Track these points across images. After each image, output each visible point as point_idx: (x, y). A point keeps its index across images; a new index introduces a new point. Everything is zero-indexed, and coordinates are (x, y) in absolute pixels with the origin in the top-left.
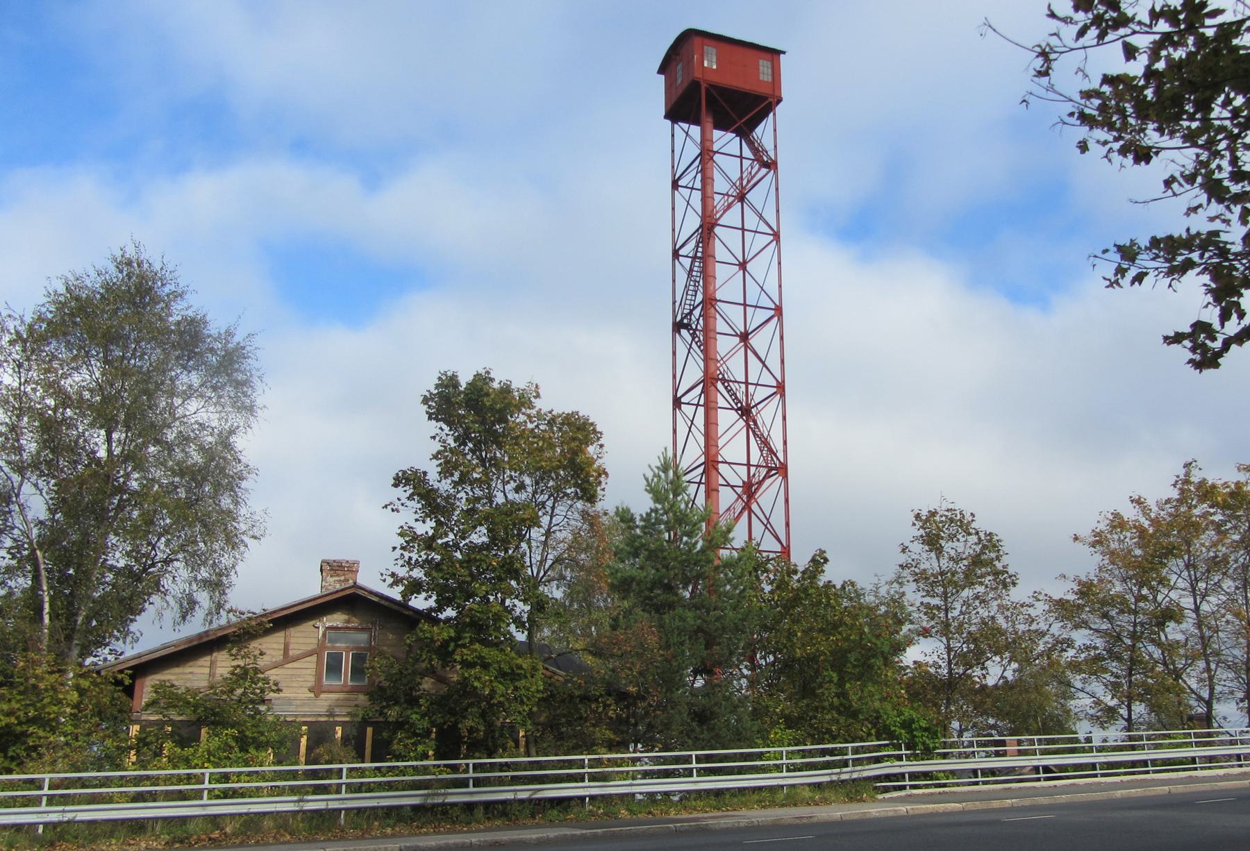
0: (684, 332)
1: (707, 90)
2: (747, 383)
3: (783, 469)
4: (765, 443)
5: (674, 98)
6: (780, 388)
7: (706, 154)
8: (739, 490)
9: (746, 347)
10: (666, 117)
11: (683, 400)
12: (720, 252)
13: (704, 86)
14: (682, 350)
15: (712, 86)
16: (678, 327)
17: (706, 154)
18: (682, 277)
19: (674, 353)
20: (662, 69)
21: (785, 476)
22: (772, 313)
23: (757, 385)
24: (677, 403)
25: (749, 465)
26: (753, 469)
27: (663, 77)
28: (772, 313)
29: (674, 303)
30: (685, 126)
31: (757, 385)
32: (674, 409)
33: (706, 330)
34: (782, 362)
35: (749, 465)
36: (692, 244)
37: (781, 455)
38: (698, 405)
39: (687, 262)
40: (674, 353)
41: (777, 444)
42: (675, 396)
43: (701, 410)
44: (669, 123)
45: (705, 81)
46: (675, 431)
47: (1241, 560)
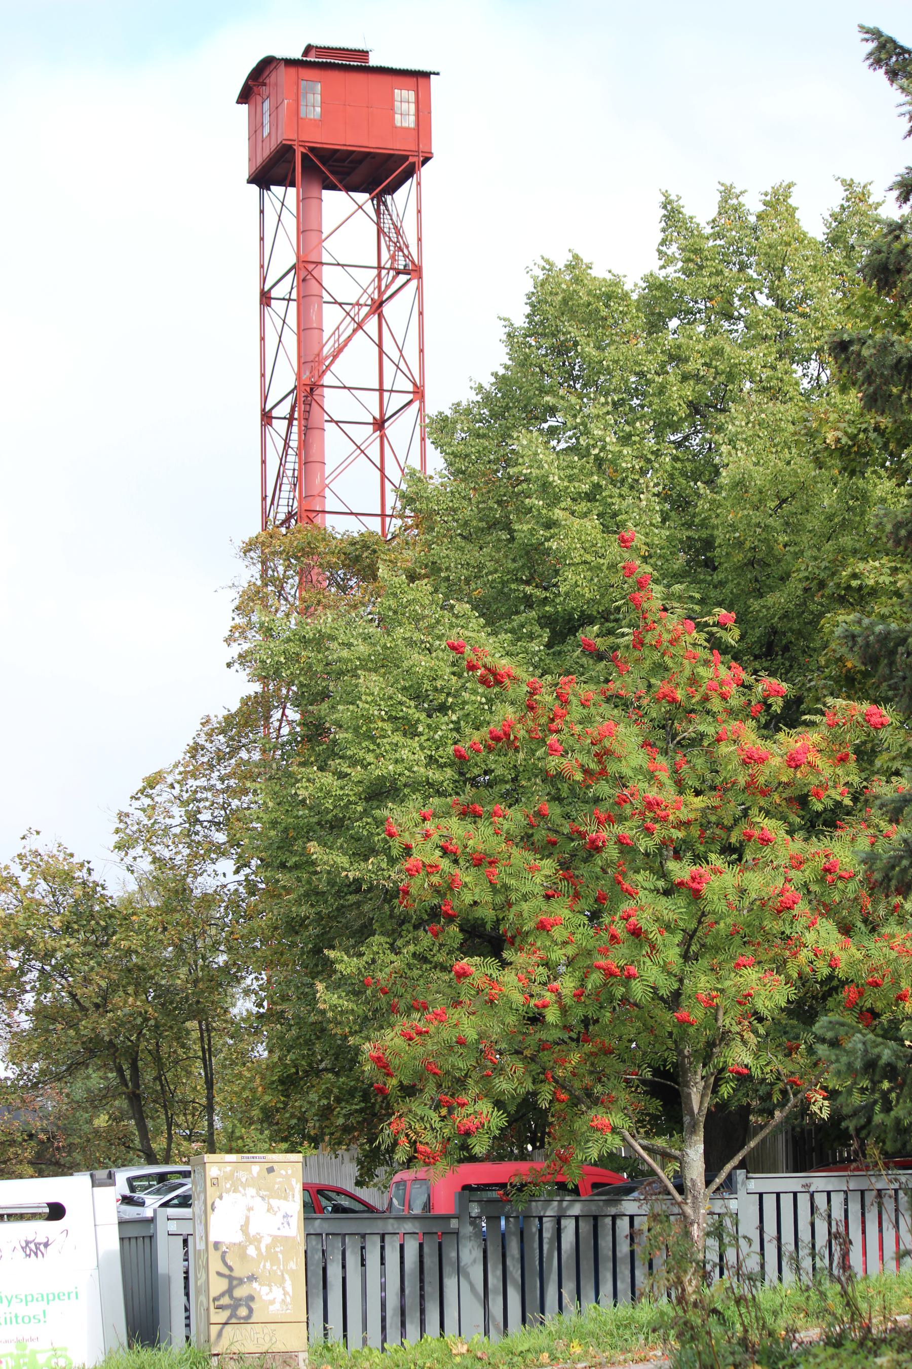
1: (304, 156)
3: (414, 271)
5: (259, 161)
7: (308, 229)
9: (382, 437)
11: (274, 294)
12: (334, 402)
13: (299, 151)
15: (312, 149)
17: (308, 229)
18: (275, 443)
20: (245, 96)
21: (420, 277)
22: (411, 396)
23: (391, 391)
24: (266, 298)
27: (245, 107)
28: (410, 397)
29: (264, 498)
31: (391, 391)
32: (263, 426)
34: (421, 351)
35: (383, 515)
36: (289, 401)
38: (289, 300)
42: (263, 410)
43: (293, 305)
44: (255, 188)
45: (302, 143)
46: (264, 462)
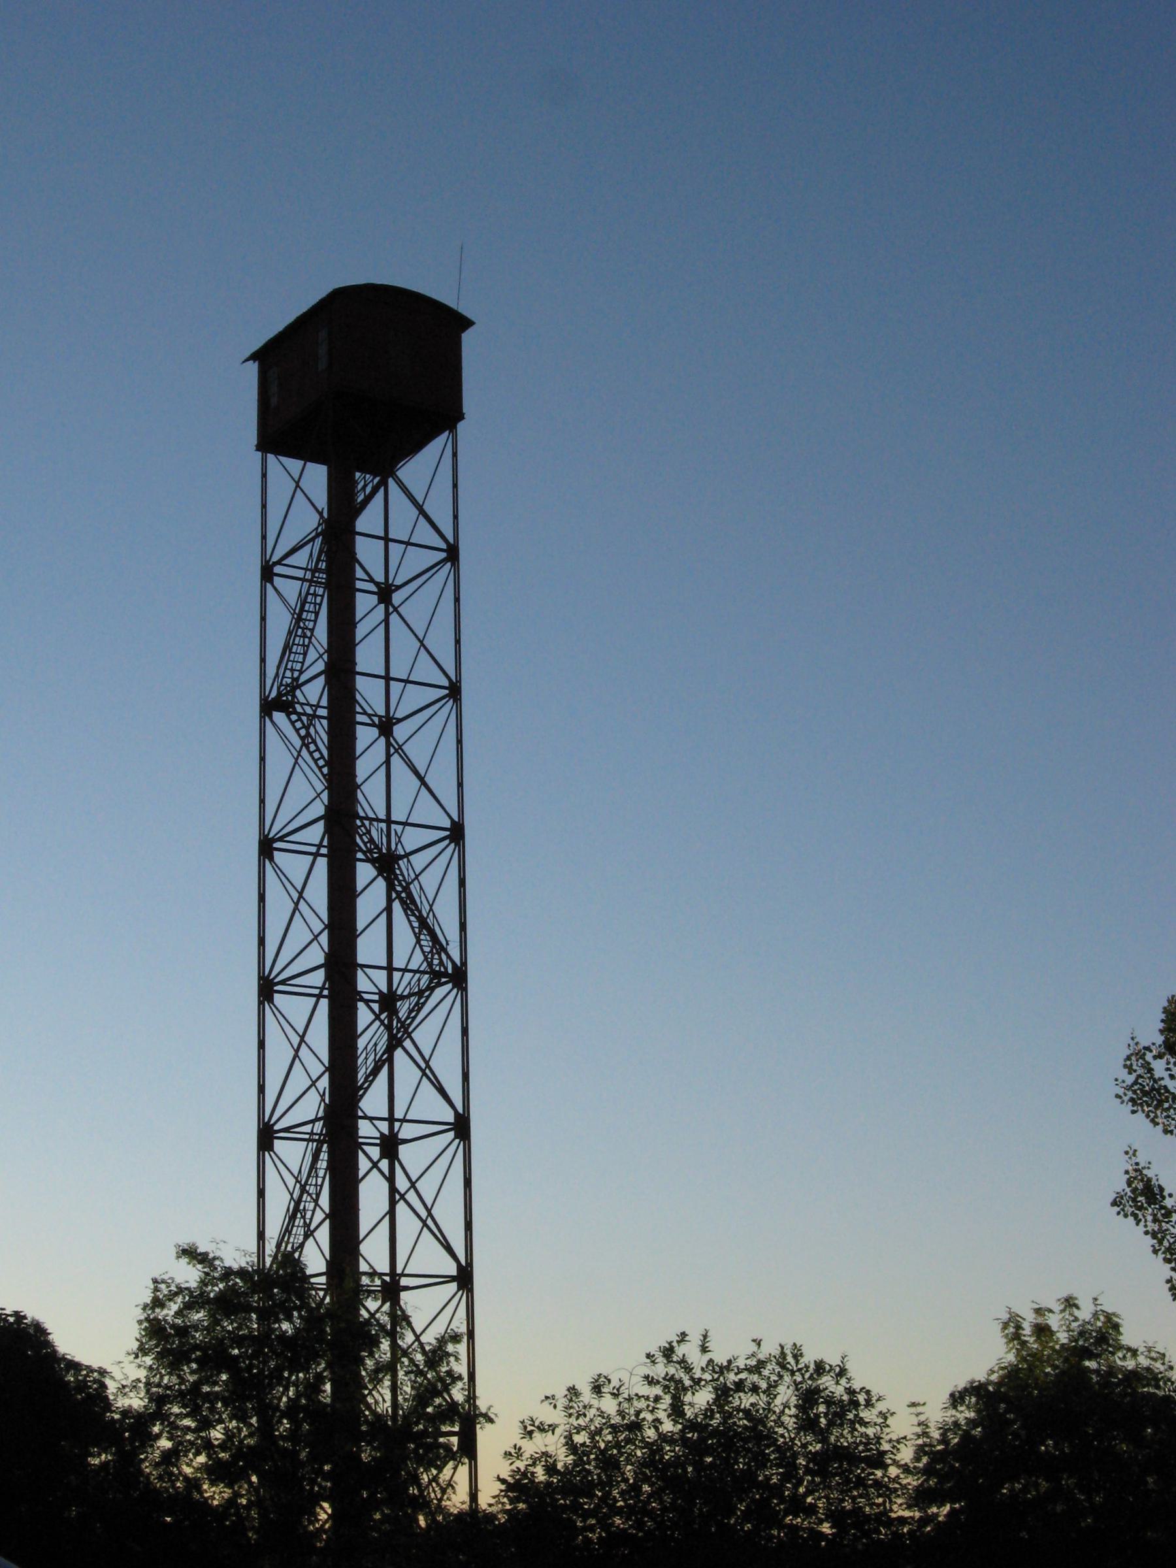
0: (279, 717)
2: (389, 821)
3: (459, 978)
4: (424, 926)
6: (456, 833)
8: (376, 1007)
10: (257, 450)
14: (279, 758)
16: (268, 707)
18: (280, 622)
19: (261, 1193)
25: (390, 969)
26: (397, 975)
30: (295, 465)
33: (293, 1217)
35: (390, 969)
37: (454, 951)
39: (291, 590)
40: (261, 1193)
41: (449, 929)
47: (780, 1431)
